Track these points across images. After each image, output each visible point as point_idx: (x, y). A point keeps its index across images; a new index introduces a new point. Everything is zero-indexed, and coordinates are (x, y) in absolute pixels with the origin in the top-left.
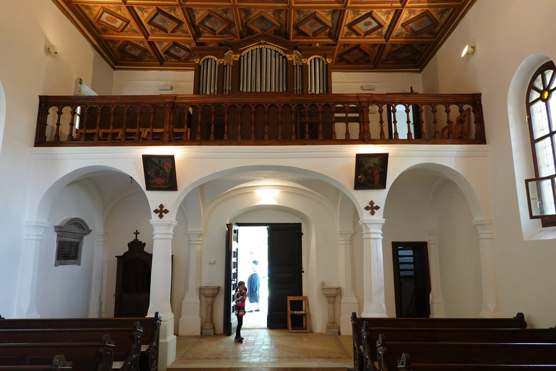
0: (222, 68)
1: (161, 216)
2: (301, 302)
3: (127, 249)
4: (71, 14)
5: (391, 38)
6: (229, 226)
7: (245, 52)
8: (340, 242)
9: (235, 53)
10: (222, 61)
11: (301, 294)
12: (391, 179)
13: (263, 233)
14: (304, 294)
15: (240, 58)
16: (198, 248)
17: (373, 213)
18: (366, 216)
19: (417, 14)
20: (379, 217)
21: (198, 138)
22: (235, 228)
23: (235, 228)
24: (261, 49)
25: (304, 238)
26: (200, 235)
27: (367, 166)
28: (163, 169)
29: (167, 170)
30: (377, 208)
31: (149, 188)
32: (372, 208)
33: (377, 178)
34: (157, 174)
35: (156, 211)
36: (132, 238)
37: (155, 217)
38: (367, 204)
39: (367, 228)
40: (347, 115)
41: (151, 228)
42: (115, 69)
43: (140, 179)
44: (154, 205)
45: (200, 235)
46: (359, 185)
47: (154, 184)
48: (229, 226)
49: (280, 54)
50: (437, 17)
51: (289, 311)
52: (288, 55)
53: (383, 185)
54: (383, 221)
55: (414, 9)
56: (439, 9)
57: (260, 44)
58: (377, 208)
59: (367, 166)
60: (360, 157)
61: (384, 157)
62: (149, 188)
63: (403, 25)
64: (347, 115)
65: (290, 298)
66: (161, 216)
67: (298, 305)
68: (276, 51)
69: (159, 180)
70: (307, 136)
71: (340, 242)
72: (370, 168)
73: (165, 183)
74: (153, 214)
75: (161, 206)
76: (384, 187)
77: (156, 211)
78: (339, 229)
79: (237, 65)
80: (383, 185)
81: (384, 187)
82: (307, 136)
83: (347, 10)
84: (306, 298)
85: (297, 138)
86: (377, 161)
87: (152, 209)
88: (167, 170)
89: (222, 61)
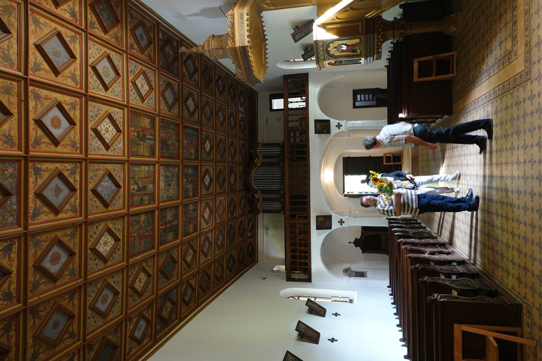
0: (264, 199)
1: (344, 222)
2: (387, 157)
3: (358, 248)
4: (221, 290)
5: (82, 26)
6: (346, 196)
7: (256, 188)
8: (354, 136)
9: (257, 193)
10: (261, 200)
11: (382, 157)
12: (325, 117)
13: (349, 179)
14: (382, 155)
15: (259, 190)
16: (357, 212)
17: (341, 126)
18: (342, 129)
19: (96, 20)
20: (342, 123)
21: (306, 207)
22: (346, 193)
23: (346, 193)
24: (254, 180)
25: (351, 156)
26: (350, 211)
27: (320, 129)
28: (323, 221)
29: (323, 219)
30: (339, 123)
31: (330, 228)
32: (339, 126)
33: (325, 124)
34: (324, 224)
35: (341, 224)
36: (353, 245)
37: (344, 225)
38: (337, 128)
39: (348, 128)
40: (292, 137)
41: (349, 227)
42: (257, 262)
43: (327, 232)
44: (338, 226)
45: (350, 211)
46: (328, 132)
47: (329, 225)
48: (346, 196)
49: (257, 170)
50: (136, 21)
51: (392, 163)
52: (258, 166)
53: (328, 121)
54: (345, 121)
55: (89, 22)
56: (129, 19)
57: (251, 180)
58: (339, 123)
59: (320, 129)
60: (317, 132)
61: (316, 121)
62: (330, 228)
63: (106, 32)
64: (292, 137)
65: (384, 163)
66: (344, 222)
67: (388, 159)
68: (255, 172)
69: (327, 223)
70: (305, 156)
71: (354, 136)
72: (321, 127)
73: (328, 220)
74: (343, 226)
75: (339, 222)
76: (329, 121)
77: (341, 224)
78: (347, 137)
79: (263, 192)
80: (328, 121)
81: (329, 121)
82: (305, 156)
83: (90, 94)
84: (384, 154)
85: (306, 161)
86: (318, 124)
87: (340, 226)
88: (323, 219)
89: (261, 200)
